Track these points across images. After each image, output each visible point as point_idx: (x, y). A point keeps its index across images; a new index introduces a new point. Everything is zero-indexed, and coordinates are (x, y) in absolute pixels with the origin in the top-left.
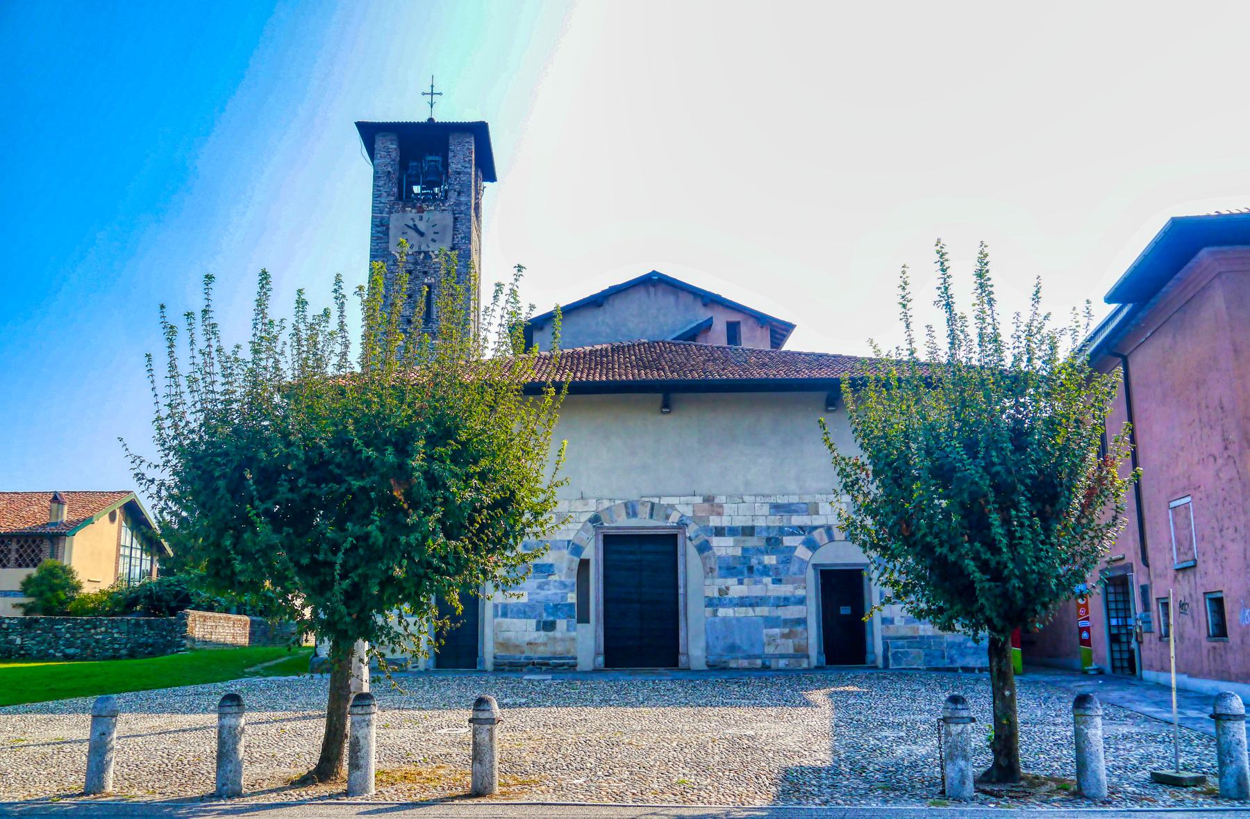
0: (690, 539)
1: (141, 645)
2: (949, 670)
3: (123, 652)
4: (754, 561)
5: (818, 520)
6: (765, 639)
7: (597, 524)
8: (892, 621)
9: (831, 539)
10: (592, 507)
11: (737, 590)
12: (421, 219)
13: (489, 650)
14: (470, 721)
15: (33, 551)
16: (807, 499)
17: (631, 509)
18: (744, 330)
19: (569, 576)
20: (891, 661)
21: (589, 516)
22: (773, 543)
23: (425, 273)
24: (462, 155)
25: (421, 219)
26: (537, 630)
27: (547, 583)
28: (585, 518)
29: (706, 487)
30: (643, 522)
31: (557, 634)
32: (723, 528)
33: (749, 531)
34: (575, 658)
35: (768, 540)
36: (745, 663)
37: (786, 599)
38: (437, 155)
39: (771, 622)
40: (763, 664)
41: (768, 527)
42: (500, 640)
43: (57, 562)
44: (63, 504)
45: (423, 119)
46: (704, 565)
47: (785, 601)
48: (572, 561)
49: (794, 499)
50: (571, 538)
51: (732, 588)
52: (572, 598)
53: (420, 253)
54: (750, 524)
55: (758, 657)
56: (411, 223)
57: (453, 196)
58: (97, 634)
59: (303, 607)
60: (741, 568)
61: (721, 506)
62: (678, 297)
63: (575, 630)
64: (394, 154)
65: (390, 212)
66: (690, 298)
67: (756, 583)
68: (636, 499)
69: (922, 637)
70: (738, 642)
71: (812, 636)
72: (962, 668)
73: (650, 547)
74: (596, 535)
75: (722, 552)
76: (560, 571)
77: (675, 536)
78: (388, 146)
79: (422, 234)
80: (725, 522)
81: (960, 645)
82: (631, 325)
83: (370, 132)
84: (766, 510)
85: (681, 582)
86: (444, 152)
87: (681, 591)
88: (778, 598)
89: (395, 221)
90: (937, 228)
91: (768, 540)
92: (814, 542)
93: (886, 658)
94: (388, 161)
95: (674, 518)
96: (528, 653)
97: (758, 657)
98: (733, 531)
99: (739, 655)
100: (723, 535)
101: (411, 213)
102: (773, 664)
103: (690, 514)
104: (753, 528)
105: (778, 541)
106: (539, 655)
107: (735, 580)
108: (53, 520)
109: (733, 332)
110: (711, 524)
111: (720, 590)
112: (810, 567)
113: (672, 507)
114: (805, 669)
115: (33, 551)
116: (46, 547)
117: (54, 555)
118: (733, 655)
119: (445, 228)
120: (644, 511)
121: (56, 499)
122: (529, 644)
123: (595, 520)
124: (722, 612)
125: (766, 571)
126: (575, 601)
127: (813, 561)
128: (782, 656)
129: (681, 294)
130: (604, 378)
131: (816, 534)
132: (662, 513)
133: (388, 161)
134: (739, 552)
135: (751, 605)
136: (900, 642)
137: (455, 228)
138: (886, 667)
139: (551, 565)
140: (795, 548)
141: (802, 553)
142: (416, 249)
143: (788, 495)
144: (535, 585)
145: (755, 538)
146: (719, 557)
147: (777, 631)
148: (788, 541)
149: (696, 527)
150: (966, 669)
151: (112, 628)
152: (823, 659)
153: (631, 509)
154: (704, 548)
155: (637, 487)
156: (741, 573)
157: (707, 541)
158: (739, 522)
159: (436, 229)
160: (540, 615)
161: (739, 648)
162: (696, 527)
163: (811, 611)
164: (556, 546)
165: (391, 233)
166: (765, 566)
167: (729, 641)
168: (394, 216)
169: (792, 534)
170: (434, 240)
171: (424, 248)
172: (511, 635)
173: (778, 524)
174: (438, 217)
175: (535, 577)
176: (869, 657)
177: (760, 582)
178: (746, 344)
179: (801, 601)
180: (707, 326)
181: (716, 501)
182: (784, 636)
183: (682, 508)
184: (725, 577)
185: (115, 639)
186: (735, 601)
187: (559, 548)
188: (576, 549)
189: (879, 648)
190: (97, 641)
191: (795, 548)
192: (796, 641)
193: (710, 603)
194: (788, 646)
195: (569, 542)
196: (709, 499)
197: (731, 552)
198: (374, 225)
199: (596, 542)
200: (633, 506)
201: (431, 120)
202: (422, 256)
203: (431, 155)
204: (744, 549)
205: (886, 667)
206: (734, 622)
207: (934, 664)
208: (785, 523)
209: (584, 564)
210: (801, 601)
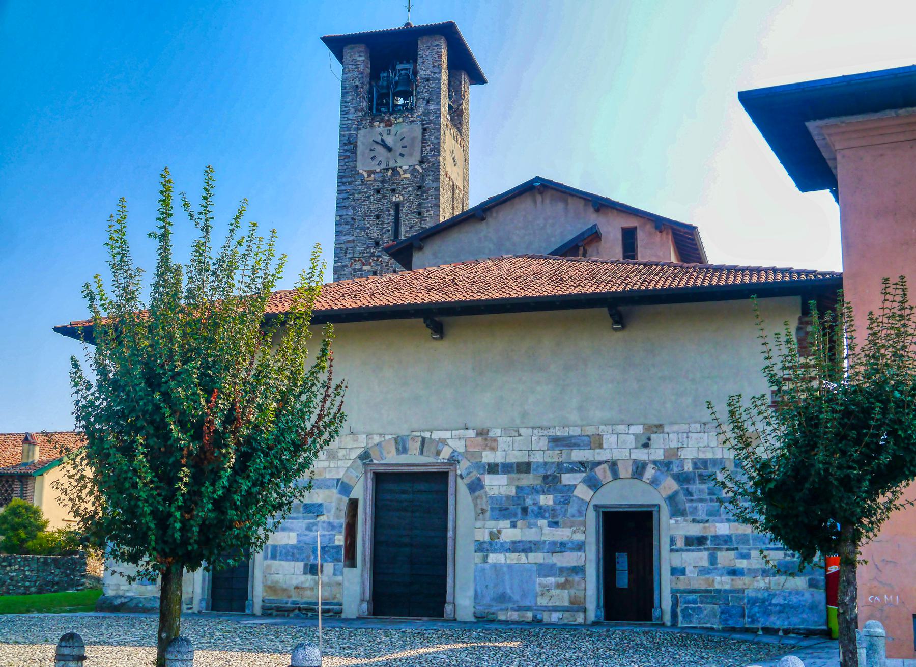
1: (48, 583)
2: (746, 630)
3: (33, 589)
4: (529, 502)
6: (538, 589)
7: (367, 461)
8: (683, 572)
9: (616, 476)
10: (362, 442)
11: (509, 534)
13: (258, 593)
14: (84, 658)
15: (7, 490)
16: (590, 430)
17: (401, 445)
18: (641, 237)
19: (338, 517)
20: (680, 618)
21: (359, 452)
22: (550, 481)
23: (393, 190)
24: (435, 60)
25: (389, 133)
26: (305, 573)
27: (315, 524)
28: (354, 454)
29: (481, 418)
30: (413, 459)
31: (323, 578)
32: (496, 465)
33: (524, 468)
34: (341, 605)
36: (515, 616)
37: (563, 544)
38: (408, 62)
39: (545, 570)
40: (535, 616)
41: (546, 463)
42: (269, 583)
43: (28, 502)
44: (34, 444)
45: (399, 25)
46: (476, 505)
47: (560, 547)
48: (341, 500)
49: (575, 431)
50: (340, 476)
51: (504, 531)
52: (340, 540)
53: (387, 169)
54: (525, 460)
55: (529, 609)
56: (379, 139)
57: (421, 107)
58: (11, 571)
60: (514, 509)
61: (495, 440)
62: (567, 203)
63: (342, 574)
64: (361, 67)
65: (358, 129)
66: (581, 203)
67: (530, 526)
68: (406, 434)
69: (718, 591)
70: (509, 591)
71: (590, 588)
72: (763, 629)
73: (407, 486)
74: (366, 473)
75: (494, 492)
76: (329, 511)
77: (446, 474)
78: (360, 57)
79: (389, 149)
80: (498, 457)
81: (764, 601)
82: (515, 239)
83: (338, 45)
84: (544, 443)
85: (450, 525)
86: (411, 56)
87: (450, 534)
88: (554, 543)
89: (363, 138)
91: (545, 477)
92: (597, 480)
93: (674, 615)
94: (356, 74)
95: (446, 454)
96: (295, 598)
97: (529, 609)
98: (507, 468)
99: (510, 606)
100: (497, 472)
101: (379, 127)
102: (547, 617)
103: (462, 450)
104: (528, 464)
105: (557, 479)
106: (305, 600)
107: (507, 523)
108: (25, 461)
109: (629, 239)
110: (484, 460)
111: (491, 533)
112: (591, 507)
113: (443, 442)
114: (580, 625)
115: (7, 490)
116: (17, 486)
117: (23, 496)
118: (503, 606)
119: (413, 139)
120: (414, 447)
121: (28, 440)
122: (297, 588)
123: (365, 456)
124: (493, 558)
125: (541, 512)
126: (342, 543)
127: (595, 501)
128: (555, 609)
129: (570, 200)
130: (787, 279)
131: (599, 471)
132: (433, 449)
133: (356, 74)
134: (512, 491)
135: (524, 551)
136: (691, 597)
137: (424, 141)
138: (674, 624)
139: (320, 505)
140: (575, 486)
141: (583, 492)
142: (383, 166)
143: (569, 426)
144: (304, 526)
145: (531, 476)
146: (492, 497)
147: (551, 580)
149: (468, 464)
150: (768, 631)
151: (25, 566)
152: (602, 613)
153: (401, 445)
154: (475, 487)
155: (408, 422)
156: (515, 515)
157: (479, 479)
158: (516, 457)
159: (404, 143)
160: (308, 558)
161: (510, 600)
162: (468, 464)
163: (590, 560)
164: (325, 485)
166: (540, 508)
167: (501, 590)
168: (362, 132)
169: (572, 471)
170: (402, 155)
172: (277, 577)
173: (556, 460)
174: (404, 130)
175: (304, 518)
176: (656, 613)
177: (536, 525)
178: (644, 254)
179: (580, 547)
180: (593, 237)
181: (491, 434)
182: (559, 586)
183: (454, 443)
184: (497, 519)
185: (26, 577)
186: (507, 546)
187: (328, 487)
188: (345, 488)
189: (667, 603)
190: (11, 579)
191: (575, 486)
192: (572, 592)
193: (481, 547)
194: (563, 598)
195: (338, 480)
196: (482, 433)
197: (504, 491)
198: (342, 144)
199: (366, 481)
200: (404, 442)
201: (408, 24)
203: (401, 63)
204: (517, 487)
205: (674, 624)
206: (505, 569)
207: (731, 623)
208: (564, 458)
210: (580, 547)
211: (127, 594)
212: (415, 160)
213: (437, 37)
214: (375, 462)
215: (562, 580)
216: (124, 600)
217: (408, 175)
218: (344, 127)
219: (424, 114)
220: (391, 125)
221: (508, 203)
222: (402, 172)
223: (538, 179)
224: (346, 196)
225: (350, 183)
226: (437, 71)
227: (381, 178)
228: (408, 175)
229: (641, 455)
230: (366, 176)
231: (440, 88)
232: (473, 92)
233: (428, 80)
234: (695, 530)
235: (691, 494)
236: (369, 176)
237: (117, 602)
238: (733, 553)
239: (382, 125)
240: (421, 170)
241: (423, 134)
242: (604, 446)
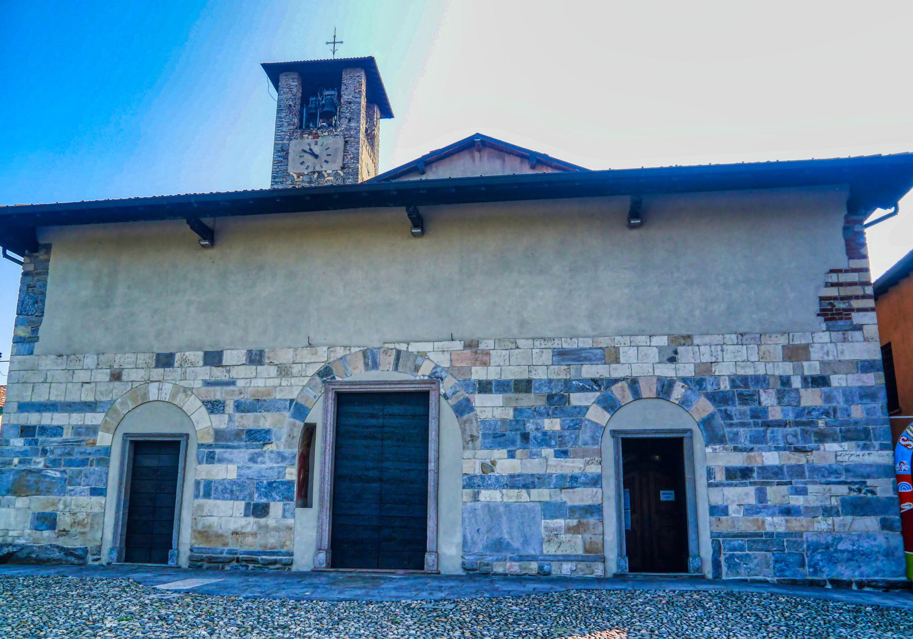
0: (446, 397)
4: (530, 426)
5: (618, 371)
25: (316, 143)
26: (246, 515)
28: (312, 370)
32: (489, 383)
33: (524, 386)
35: (550, 397)
38: (333, 89)
52: (292, 474)
53: (314, 173)
54: (525, 376)
78: (292, 83)
91: (550, 397)
95: (426, 370)
104: (529, 382)
113: (424, 355)
123: (326, 373)
124: (485, 495)
135: (526, 487)
137: (345, 151)
142: (310, 170)
147: (561, 522)
148: (577, 399)
154: (463, 409)
158: (512, 373)
159: (329, 152)
165: (290, 158)
169: (583, 389)
170: (326, 162)
171: (318, 168)
174: (328, 141)
191: (587, 408)
195: (292, 401)
202: (316, 176)
203: (328, 90)
209: (309, 431)
211: (17, 541)
213: (359, 70)
214: (338, 379)
215: (574, 522)
216: (11, 549)
218: (278, 137)
219: (346, 129)
220: (318, 137)
221: (447, 160)
223: (478, 135)
225: (282, 182)
226: (358, 96)
229: (667, 371)
230: (295, 177)
231: (359, 109)
232: (384, 124)
233: (350, 103)
234: (738, 460)
235: (730, 417)
236: (298, 177)
238: (785, 488)
239: (310, 137)
242: (622, 360)
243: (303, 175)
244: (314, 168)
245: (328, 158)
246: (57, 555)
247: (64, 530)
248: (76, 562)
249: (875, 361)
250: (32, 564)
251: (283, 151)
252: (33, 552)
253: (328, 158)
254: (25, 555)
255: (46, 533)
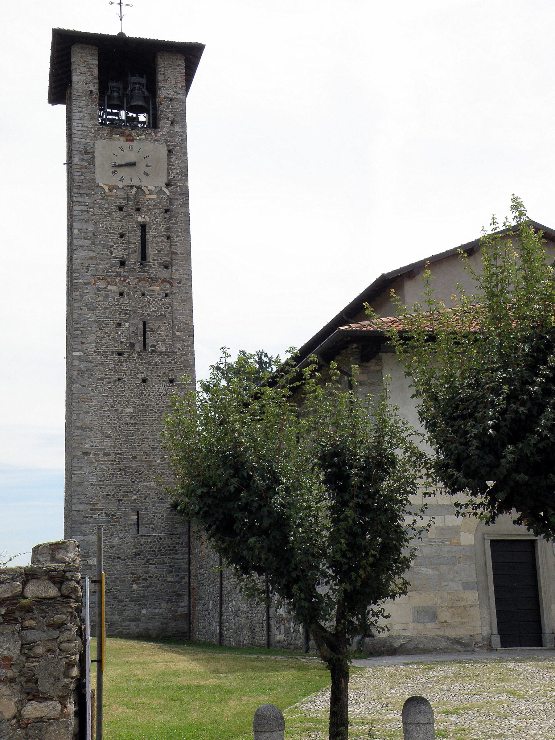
12: (131, 148)
25: (131, 148)
38: (141, 76)
45: (114, 32)
53: (132, 187)
59: (364, 520)
65: (96, 139)
90: (554, 224)
137: (170, 163)
142: (126, 182)
159: (148, 161)
165: (98, 161)
170: (146, 174)
171: (136, 182)
202: (134, 190)
203: (133, 75)
211: (403, 634)
212: (161, 182)
216: (403, 641)
217: (154, 196)
222: (147, 192)
224: (85, 208)
225: (88, 195)
227: (124, 196)
228: (154, 196)
230: (107, 190)
236: (111, 191)
237: (397, 644)
239: (122, 139)
240: (168, 193)
241: (169, 155)
243: (117, 188)
244: (131, 181)
245: (147, 170)
246: (443, 644)
247: (446, 622)
248: (462, 649)
249: (192, 371)
250: (420, 654)
251: (87, 153)
252: (421, 643)
253: (147, 170)
254: (412, 647)
255: (430, 625)
